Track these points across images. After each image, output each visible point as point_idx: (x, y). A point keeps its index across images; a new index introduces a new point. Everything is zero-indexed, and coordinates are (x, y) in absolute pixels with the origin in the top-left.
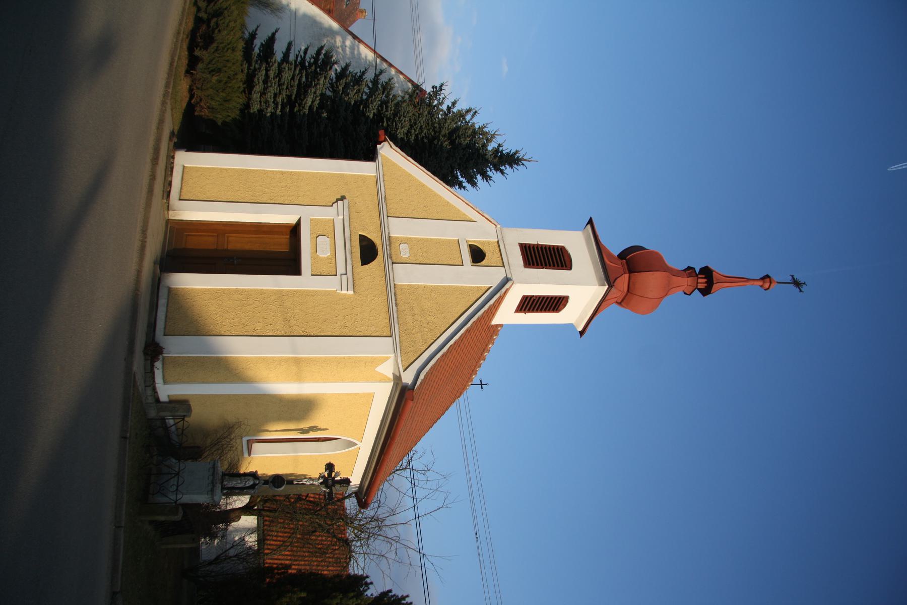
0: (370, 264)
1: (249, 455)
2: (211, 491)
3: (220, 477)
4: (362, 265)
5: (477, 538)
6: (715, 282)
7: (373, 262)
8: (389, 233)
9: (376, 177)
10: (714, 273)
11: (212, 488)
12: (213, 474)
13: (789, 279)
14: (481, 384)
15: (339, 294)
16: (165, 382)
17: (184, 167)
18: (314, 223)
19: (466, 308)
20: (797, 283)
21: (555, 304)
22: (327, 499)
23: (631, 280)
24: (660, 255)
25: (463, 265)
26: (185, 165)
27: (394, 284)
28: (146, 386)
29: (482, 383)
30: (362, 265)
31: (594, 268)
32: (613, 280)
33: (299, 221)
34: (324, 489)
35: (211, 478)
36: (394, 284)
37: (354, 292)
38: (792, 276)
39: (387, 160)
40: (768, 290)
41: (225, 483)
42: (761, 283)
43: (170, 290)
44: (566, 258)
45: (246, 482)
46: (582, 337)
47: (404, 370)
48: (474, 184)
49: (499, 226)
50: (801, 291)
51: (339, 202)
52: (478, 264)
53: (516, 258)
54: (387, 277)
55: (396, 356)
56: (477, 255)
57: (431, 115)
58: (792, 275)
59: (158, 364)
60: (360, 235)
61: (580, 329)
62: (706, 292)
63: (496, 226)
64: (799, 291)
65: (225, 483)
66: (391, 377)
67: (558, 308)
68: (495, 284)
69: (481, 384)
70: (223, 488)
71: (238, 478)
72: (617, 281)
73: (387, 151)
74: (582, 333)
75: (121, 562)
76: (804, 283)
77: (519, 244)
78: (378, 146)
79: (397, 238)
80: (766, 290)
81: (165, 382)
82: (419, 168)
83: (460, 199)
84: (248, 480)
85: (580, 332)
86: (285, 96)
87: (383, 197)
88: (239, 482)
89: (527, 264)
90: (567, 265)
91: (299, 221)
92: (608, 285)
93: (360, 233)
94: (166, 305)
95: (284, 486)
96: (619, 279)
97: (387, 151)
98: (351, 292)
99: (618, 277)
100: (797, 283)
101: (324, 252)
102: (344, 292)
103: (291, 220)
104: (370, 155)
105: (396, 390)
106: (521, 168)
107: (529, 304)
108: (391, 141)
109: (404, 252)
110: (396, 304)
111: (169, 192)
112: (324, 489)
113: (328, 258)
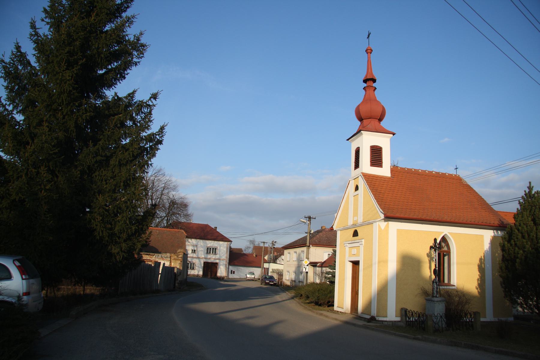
1: (455, 286)
8: (351, 225)
15: (364, 245)
16: (386, 317)
17: (337, 307)
23: (366, 118)
24: (356, 109)
31: (359, 137)
33: (350, 261)
43: (362, 313)
46: (396, 133)
49: (350, 180)
54: (361, 225)
55: (377, 221)
56: (357, 188)
59: (377, 318)
60: (353, 237)
61: (392, 135)
62: (374, 81)
63: (350, 181)
65: (435, 295)
66: (386, 223)
74: (394, 134)
75: (159, 280)
81: (386, 317)
83: (344, 196)
87: (343, 228)
91: (350, 261)
92: (361, 131)
98: (363, 240)
102: (363, 243)
103: (351, 264)
105: (391, 220)
109: (355, 219)
110: (366, 222)
111: (341, 312)
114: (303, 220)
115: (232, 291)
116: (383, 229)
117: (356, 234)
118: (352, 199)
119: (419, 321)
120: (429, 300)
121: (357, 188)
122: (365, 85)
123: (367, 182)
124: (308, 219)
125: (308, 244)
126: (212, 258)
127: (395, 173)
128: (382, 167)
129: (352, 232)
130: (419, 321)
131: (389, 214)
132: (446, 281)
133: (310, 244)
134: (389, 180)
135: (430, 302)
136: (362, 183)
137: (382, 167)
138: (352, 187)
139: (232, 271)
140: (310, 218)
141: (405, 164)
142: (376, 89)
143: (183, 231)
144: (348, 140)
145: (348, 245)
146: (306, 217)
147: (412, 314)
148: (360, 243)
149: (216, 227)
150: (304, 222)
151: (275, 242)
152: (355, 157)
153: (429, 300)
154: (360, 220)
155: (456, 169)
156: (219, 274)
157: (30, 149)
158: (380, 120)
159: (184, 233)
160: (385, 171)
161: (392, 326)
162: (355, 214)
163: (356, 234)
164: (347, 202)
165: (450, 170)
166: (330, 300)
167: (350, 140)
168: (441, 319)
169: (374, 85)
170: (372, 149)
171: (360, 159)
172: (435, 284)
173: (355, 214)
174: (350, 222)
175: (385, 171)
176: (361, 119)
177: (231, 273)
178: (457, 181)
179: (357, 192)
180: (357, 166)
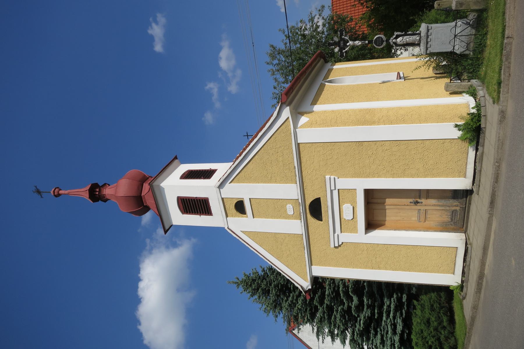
0: (314, 198)
2: (429, 30)
3: (422, 42)
4: (320, 198)
5: (253, 46)
6: (88, 191)
7: (312, 200)
8: (301, 222)
9: (312, 265)
10: (88, 197)
11: (428, 32)
12: (427, 43)
13: (44, 195)
14: (248, 136)
17: (454, 274)
18: (354, 230)
19: (247, 167)
20: (39, 192)
21: (190, 175)
22: (343, 30)
25: (250, 199)
26: (453, 275)
27: (296, 184)
28: (484, 96)
29: (247, 137)
30: (320, 198)
32: (150, 191)
34: (346, 38)
35: (429, 40)
36: (296, 184)
37: (325, 177)
38: (42, 197)
39: (305, 279)
40: (56, 187)
41: (418, 38)
42: (61, 192)
44: (181, 205)
45: (402, 40)
47: (289, 117)
48: (263, 270)
50: (36, 187)
51: (338, 246)
52: (239, 200)
53: (215, 205)
56: (240, 207)
57: (267, 310)
58: (42, 198)
60: (321, 220)
64: (37, 187)
67: (189, 172)
68: (228, 185)
69: (248, 136)
70: (420, 34)
71: (408, 42)
72: (148, 191)
73: (305, 284)
74: (176, 158)
76: (34, 192)
77: (212, 216)
78: (310, 287)
79: (296, 218)
80: (58, 188)
82: (263, 256)
84: (401, 41)
85: (177, 159)
86: (317, 297)
88: (407, 40)
89: (207, 200)
90: (180, 200)
93: (322, 222)
94: (468, 163)
95: (374, 39)
96: (147, 192)
97: (305, 284)
99: (148, 192)
100: (39, 192)
101: (347, 209)
104: (317, 282)
106: (242, 277)
107: (207, 174)
108: (301, 291)
112: (346, 38)
113: (344, 203)
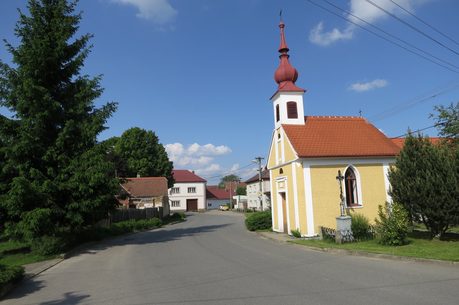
56: (279, 136)
60: (280, 174)
114: (254, 161)
115: (153, 232)
116: (299, 167)
117: (281, 172)
118: (277, 145)
119: (332, 235)
120: (339, 219)
121: (279, 136)
122: (280, 54)
123: (285, 132)
124: (258, 160)
125: (260, 179)
126: (192, 196)
127: (309, 121)
128: (297, 118)
129: (278, 170)
130: (332, 235)
131: (301, 155)
132: (355, 202)
133: (262, 178)
134: (303, 128)
135: (339, 220)
136: (282, 132)
137: (297, 118)
138: (276, 136)
139: (209, 204)
140: (260, 159)
141: (311, 115)
142: (289, 56)
143: (165, 178)
144: (270, 99)
145: (277, 180)
146: (257, 158)
147: (326, 231)
148: (285, 179)
149: (194, 172)
150: (255, 162)
151: (240, 178)
152: (277, 111)
153: (339, 219)
154: (283, 162)
155: (360, 112)
156: (233, 197)
157: (98, 114)
158: (294, 80)
159: (166, 179)
160: (300, 121)
161: (312, 240)
162: (280, 156)
163: (281, 172)
164: (274, 146)
165: (353, 114)
166: (271, 222)
167: (272, 99)
168: (348, 233)
169: (288, 53)
170: (288, 105)
171: (280, 114)
172: (342, 205)
173: (280, 156)
174: (277, 164)
175: (300, 121)
176: (279, 82)
177: (209, 206)
178: (360, 122)
179: (280, 139)
180: (278, 119)
